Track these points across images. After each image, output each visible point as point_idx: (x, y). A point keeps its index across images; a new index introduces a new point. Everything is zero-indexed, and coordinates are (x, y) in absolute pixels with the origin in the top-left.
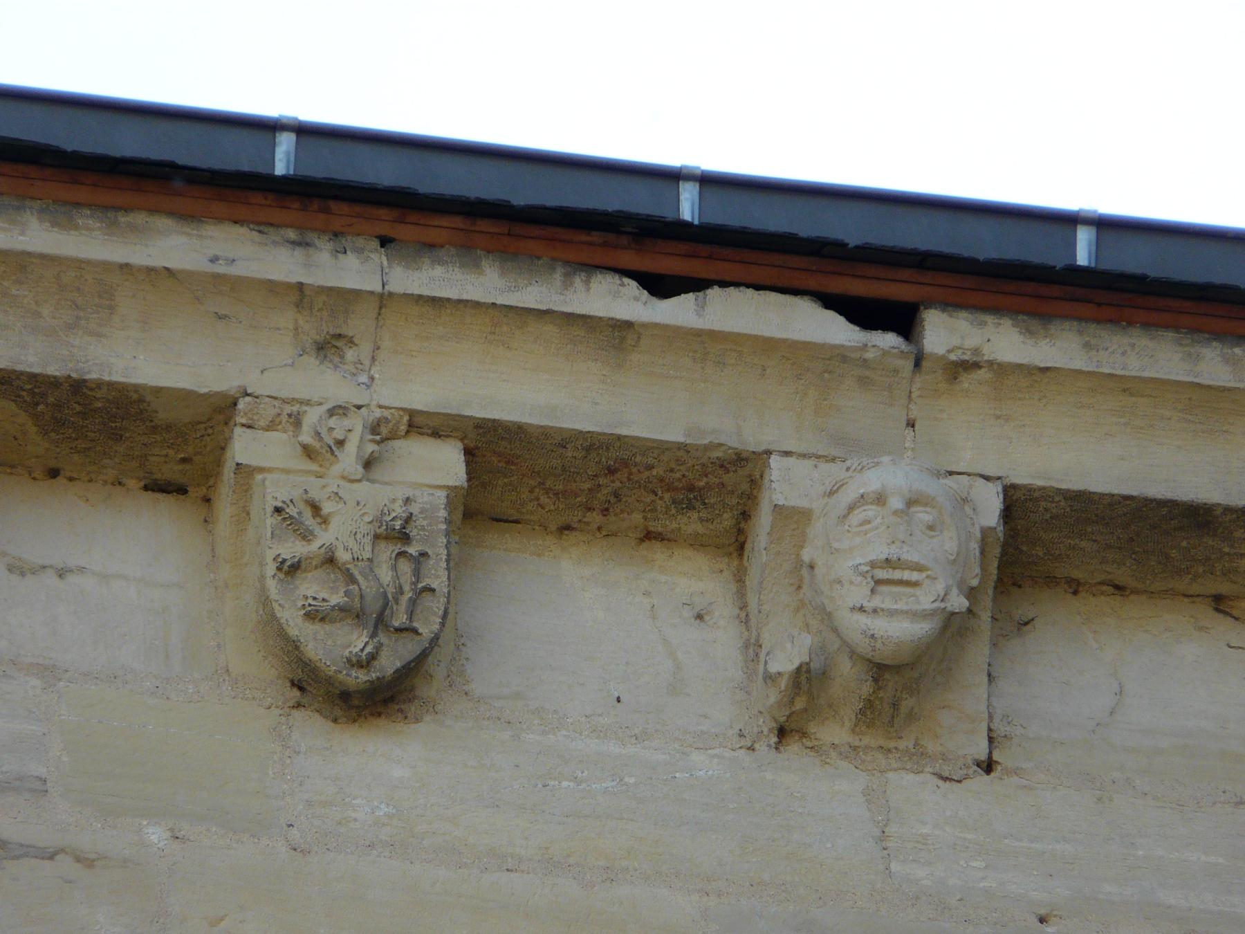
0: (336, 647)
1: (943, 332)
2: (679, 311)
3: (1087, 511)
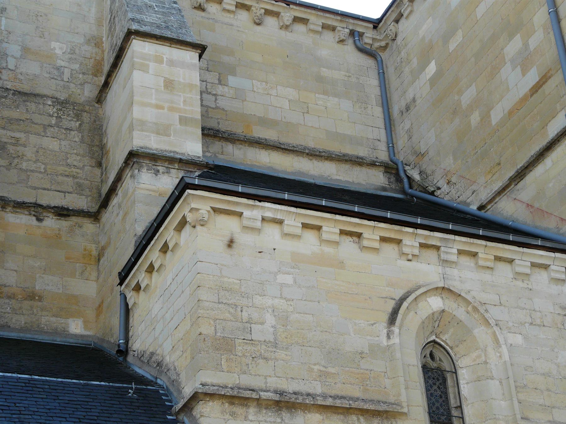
0: (257, 21)
1: (291, 6)
2: (277, 3)
3: (298, 17)
